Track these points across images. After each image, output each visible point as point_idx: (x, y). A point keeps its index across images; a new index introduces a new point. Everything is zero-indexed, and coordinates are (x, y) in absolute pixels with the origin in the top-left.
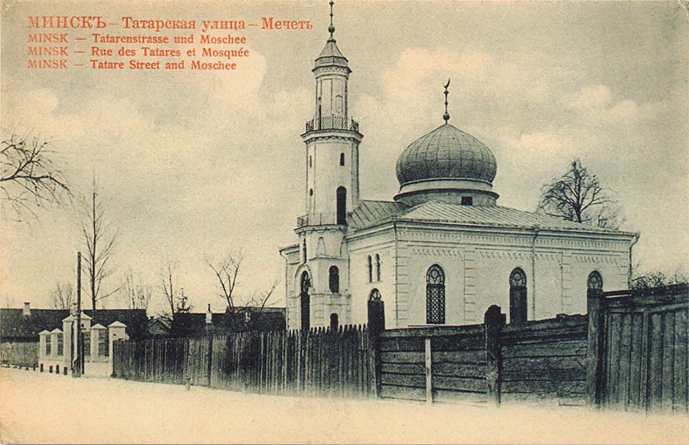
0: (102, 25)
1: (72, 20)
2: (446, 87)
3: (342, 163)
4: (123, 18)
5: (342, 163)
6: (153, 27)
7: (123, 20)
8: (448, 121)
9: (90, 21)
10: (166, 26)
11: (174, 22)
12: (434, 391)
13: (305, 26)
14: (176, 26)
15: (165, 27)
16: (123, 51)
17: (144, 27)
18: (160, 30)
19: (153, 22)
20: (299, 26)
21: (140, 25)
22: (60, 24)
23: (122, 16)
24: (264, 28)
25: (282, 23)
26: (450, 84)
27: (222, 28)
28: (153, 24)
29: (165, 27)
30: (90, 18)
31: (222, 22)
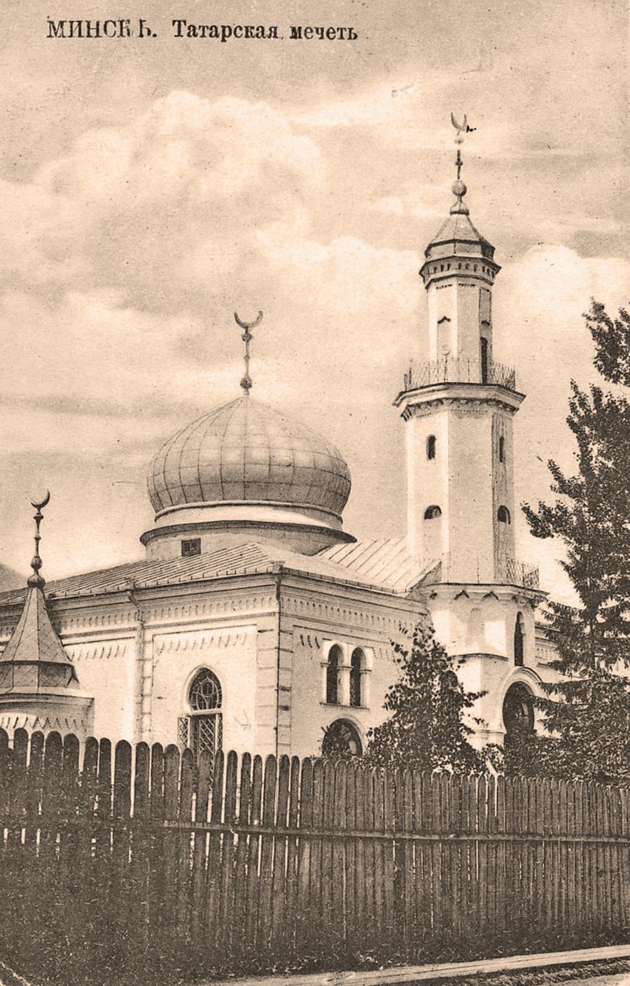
0: (353, 36)
3: (431, 454)
4: (174, 22)
5: (431, 454)
6: (217, 36)
7: (173, 25)
10: (235, 34)
12: (137, 310)
13: (346, 34)
16: (224, 36)
17: (203, 36)
18: (226, 39)
19: (216, 28)
20: (338, 34)
21: (200, 32)
22: (91, 31)
23: (391, 97)
24: (50, 36)
25: (315, 30)
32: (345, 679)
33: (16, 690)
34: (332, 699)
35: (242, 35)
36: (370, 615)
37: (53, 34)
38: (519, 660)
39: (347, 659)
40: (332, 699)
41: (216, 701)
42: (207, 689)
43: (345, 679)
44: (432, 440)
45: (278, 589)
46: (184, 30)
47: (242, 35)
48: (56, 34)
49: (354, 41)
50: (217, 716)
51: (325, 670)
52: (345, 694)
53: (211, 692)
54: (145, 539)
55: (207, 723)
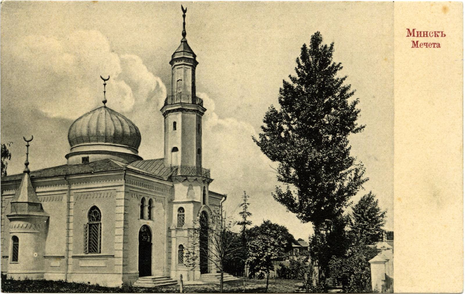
0: (443, 35)
1: (430, 33)
8: (106, 104)
9: (438, 34)
11: (435, 32)
14: (436, 35)
20: (433, 45)
30: (438, 32)
32: (146, 209)
33: (19, 213)
34: (142, 217)
35: (433, 35)
36: (149, 185)
38: (204, 203)
40: (142, 217)
41: (98, 218)
42: (95, 213)
43: (146, 209)
45: (125, 176)
47: (433, 35)
48: (411, 34)
49: (444, 37)
50: (99, 224)
51: (140, 206)
52: (146, 214)
53: (96, 215)
54: (67, 157)
55: (95, 226)
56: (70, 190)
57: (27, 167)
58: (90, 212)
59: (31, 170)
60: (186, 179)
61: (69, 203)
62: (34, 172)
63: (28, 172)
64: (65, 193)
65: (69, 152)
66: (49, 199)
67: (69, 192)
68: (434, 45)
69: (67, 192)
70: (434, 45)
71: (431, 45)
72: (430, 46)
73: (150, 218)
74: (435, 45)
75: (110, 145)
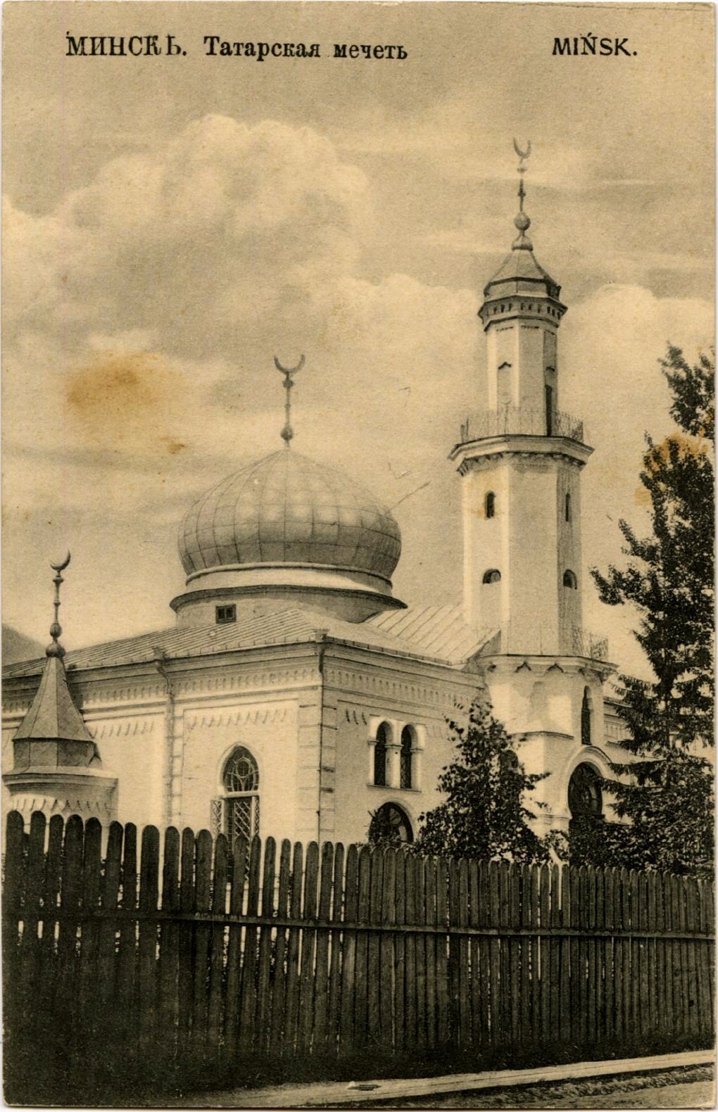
0: (402, 55)
2: (60, 569)
4: (206, 38)
6: (253, 53)
7: (205, 42)
11: (286, 45)
15: (270, 52)
20: (386, 53)
24: (70, 54)
25: (360, 49)
26: (70, 565)
27: (112, 53)
28: (252, 49)
29: (270, 52)
31: (93, 39)
32: (395, 760)
34: (380, 780)
37: (73, 51)
38: (586, 739)
39: (396, 737)
40: (380, 780)
41: (251, 783)
42: (243, 768)
43: (395, 760)
44: (490, 498)
46: (217, 48)
48: (76, 50)
50: (253, 799)
56: (173, 702)
57: (55, 640)
58: (229, 764)
59: (68, 649)
60: (525, 664)
61: (171, 740)
62: (79, 652)
63: (59, 654)
64: (163, 713)
65: (184, 590)
66: (132, 728)
67: (172, 711)
68: (390, 51)
69: (163, 709)
70: (390, 51)
71: (382, 50)
72: (379, 54)
73: (407, 783)
74: (393, 49)
75: (300, 567)
